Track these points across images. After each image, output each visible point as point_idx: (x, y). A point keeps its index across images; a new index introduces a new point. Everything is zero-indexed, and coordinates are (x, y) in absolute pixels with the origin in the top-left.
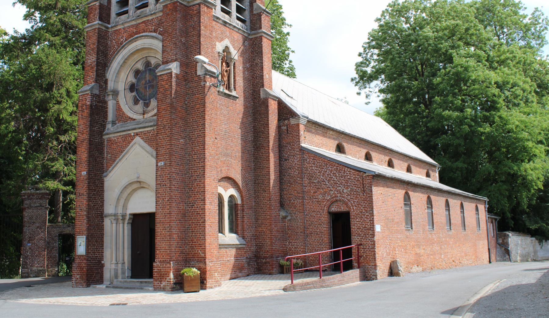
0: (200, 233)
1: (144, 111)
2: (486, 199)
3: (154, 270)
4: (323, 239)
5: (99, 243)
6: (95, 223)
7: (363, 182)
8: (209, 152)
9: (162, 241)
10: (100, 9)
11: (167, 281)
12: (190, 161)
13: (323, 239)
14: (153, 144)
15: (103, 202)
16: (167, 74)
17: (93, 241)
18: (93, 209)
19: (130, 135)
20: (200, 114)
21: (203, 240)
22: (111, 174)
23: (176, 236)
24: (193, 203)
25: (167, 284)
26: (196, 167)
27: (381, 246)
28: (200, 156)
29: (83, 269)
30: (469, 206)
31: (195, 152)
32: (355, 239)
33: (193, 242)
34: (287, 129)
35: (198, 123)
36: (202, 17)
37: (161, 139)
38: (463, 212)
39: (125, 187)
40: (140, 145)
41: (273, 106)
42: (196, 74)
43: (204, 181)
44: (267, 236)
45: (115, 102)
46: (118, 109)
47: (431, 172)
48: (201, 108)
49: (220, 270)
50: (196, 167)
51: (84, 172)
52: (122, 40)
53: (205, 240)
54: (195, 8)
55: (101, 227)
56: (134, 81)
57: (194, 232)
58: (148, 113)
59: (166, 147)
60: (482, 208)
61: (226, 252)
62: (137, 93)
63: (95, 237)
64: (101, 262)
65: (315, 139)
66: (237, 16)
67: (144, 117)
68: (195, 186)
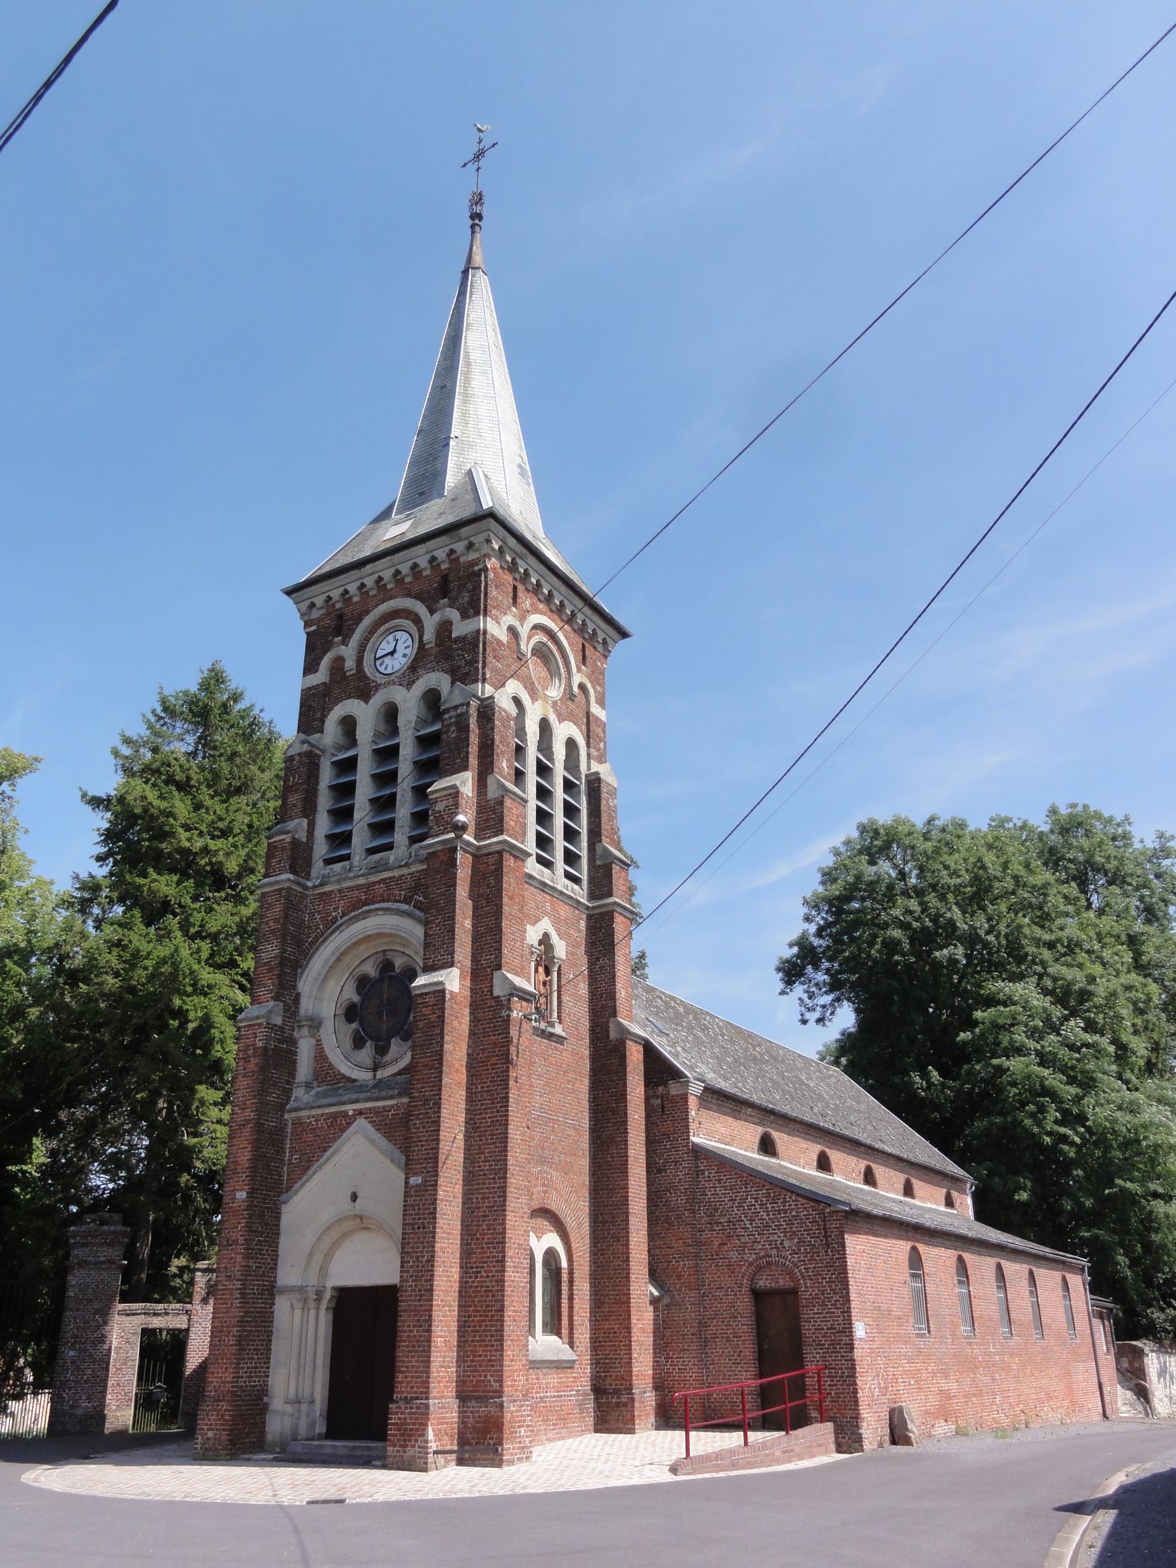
0: (492, 1336)
1: (374, 1062)
2: (1084, 1262)
3: (391, 1419)
4: (741, 1352)
5: (262, 1354)
6: (256, 1308)
7: (825, 1225)
8: (514, 1157)
9: (412, 1352)
10: (292, 849)
11: (419, 1447)
12: (474, 1176)
13: (741, 1352)
14: (394, 1136)
15: (275, 1258)
16: (434, 992)
17: (250, 1350)
18: (256, 1275)
19: (344, 1114)
20: (499, 1077)
21: (497, 1350)
22: (297, 1198)
23: (441, 1342)
24: (477, 1267)
25: (419, 1452)
26: (487, 1188)
27: (867, 1372)
28: (496, 1165)
29: (222, 1415)
30: (1048, 1278)
31: (485, 1157)
32: (813, 1358)
33: (474, 1356)
34: (663, 1105)
35: (493, 1095)
36: (505, 878)
37: (418, 1128)
38: (1034, 1292)
39: (329, 1228)
40: (367, 1137)
41: (635, 1056)
42: (492, 994)
43: (504, 1220)
44: (621, 1341)
45: (313, 1041)
46: (320, 1056)
47: (955, 1194)
48: (502, 1063)
49: (531, 1421)
50: (487, 1188)
51: (240, 1193)
52: (334, 914)
53: (503, 1350)
54: (492, 860)
55: (269, 1317)
56: (356, 998)
57: (479, 1331)
58: (384, 1067)
59: (428, 1145)
60: (1077, 1282)
61: (538, 1379)
62: (361, 1025)
63: (255, 1341)
64: (262, 1400)
65: (718, 1126)
66: (565, 871)
67: (375, 1075)
68: (483, 1230)
